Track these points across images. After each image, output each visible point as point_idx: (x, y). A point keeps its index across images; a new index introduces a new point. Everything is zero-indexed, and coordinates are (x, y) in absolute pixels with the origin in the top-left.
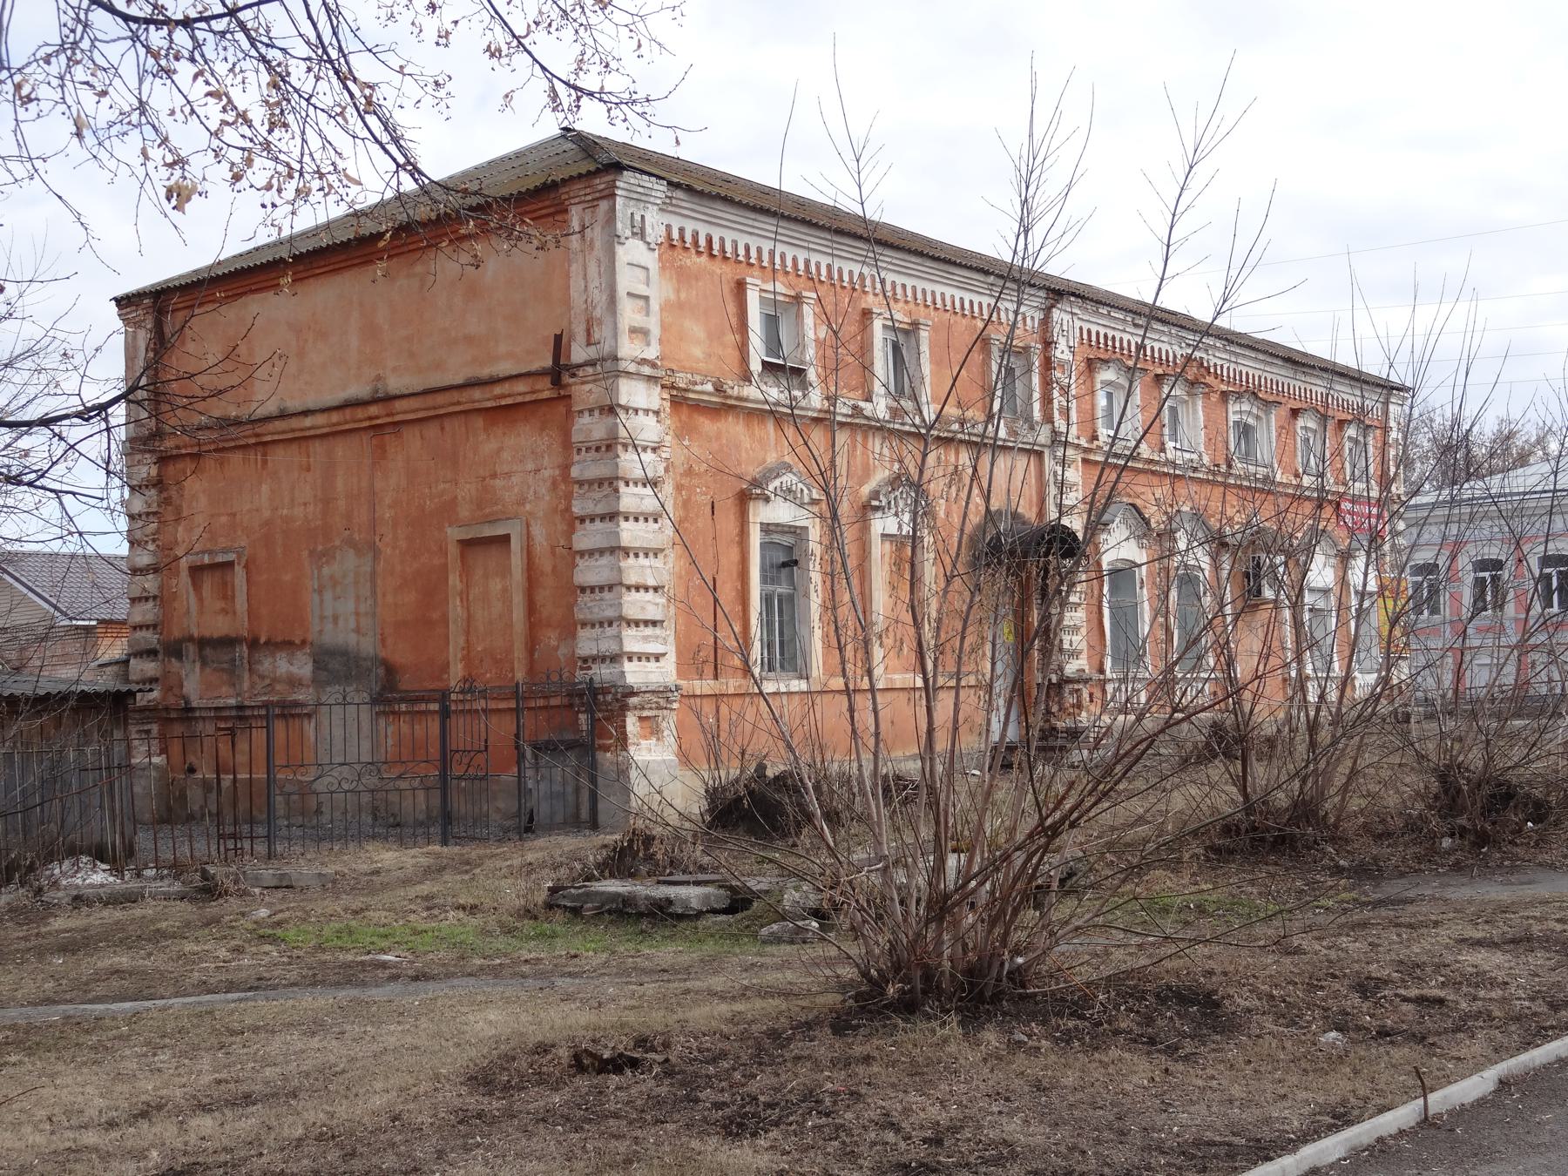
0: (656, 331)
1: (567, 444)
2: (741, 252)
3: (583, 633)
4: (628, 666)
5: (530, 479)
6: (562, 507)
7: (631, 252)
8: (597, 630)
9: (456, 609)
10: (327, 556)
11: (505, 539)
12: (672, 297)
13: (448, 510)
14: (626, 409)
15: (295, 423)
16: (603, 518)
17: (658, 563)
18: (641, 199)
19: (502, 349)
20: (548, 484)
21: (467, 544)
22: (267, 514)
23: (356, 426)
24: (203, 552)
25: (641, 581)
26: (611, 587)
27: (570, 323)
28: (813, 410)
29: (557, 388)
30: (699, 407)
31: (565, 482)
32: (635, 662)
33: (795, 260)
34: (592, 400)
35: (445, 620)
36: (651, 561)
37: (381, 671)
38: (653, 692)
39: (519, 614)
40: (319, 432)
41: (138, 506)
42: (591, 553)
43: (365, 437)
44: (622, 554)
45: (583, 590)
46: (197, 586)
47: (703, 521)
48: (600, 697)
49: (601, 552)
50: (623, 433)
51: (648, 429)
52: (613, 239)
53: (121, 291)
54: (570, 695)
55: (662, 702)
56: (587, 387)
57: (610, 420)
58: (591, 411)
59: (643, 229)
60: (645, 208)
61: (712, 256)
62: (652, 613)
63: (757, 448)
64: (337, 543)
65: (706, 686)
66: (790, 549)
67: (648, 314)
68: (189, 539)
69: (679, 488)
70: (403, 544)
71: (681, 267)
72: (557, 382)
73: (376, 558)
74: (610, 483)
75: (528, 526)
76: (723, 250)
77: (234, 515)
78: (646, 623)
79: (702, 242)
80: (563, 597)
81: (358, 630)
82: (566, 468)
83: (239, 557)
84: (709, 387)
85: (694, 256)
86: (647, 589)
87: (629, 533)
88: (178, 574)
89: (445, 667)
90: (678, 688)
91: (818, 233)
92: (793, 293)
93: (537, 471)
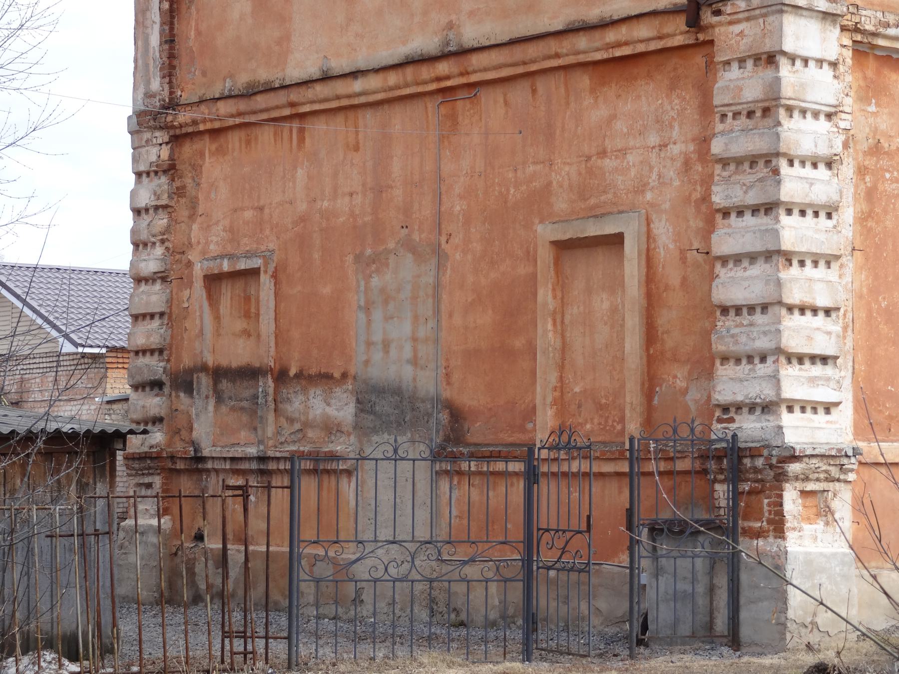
1: (706, 108)
3: (724, 372)
4: (787, 419)
5: (653, 157)
6: (696, 195)
8: (745, 367)
9: (546, 335)
10: (372, 263)
11: (617, 240)
13: (538, 201)
14: (793, 58)
16: (755, 210)
17: (832, 275)
20: (678, 164)
25: (808, 300)
26: (765, 308)
34: (743, 46)
36: (821, 272)
37: (444, 417)
38: (822, 456)
39: (633, 343)
42: (737, 259)
44: (782, 261)
45: (725, 310)
48: (747, 462)
49: (753, 257)
50: (787, 91)
55: (835, 472)
56: (737, 29)
69: (861, 171)
74: (768, 161)
75: (648, 222)
81: (414, 361)
82: (704, 142)
86: (815, 311)
89: (530, 413)
93: (663, 146)
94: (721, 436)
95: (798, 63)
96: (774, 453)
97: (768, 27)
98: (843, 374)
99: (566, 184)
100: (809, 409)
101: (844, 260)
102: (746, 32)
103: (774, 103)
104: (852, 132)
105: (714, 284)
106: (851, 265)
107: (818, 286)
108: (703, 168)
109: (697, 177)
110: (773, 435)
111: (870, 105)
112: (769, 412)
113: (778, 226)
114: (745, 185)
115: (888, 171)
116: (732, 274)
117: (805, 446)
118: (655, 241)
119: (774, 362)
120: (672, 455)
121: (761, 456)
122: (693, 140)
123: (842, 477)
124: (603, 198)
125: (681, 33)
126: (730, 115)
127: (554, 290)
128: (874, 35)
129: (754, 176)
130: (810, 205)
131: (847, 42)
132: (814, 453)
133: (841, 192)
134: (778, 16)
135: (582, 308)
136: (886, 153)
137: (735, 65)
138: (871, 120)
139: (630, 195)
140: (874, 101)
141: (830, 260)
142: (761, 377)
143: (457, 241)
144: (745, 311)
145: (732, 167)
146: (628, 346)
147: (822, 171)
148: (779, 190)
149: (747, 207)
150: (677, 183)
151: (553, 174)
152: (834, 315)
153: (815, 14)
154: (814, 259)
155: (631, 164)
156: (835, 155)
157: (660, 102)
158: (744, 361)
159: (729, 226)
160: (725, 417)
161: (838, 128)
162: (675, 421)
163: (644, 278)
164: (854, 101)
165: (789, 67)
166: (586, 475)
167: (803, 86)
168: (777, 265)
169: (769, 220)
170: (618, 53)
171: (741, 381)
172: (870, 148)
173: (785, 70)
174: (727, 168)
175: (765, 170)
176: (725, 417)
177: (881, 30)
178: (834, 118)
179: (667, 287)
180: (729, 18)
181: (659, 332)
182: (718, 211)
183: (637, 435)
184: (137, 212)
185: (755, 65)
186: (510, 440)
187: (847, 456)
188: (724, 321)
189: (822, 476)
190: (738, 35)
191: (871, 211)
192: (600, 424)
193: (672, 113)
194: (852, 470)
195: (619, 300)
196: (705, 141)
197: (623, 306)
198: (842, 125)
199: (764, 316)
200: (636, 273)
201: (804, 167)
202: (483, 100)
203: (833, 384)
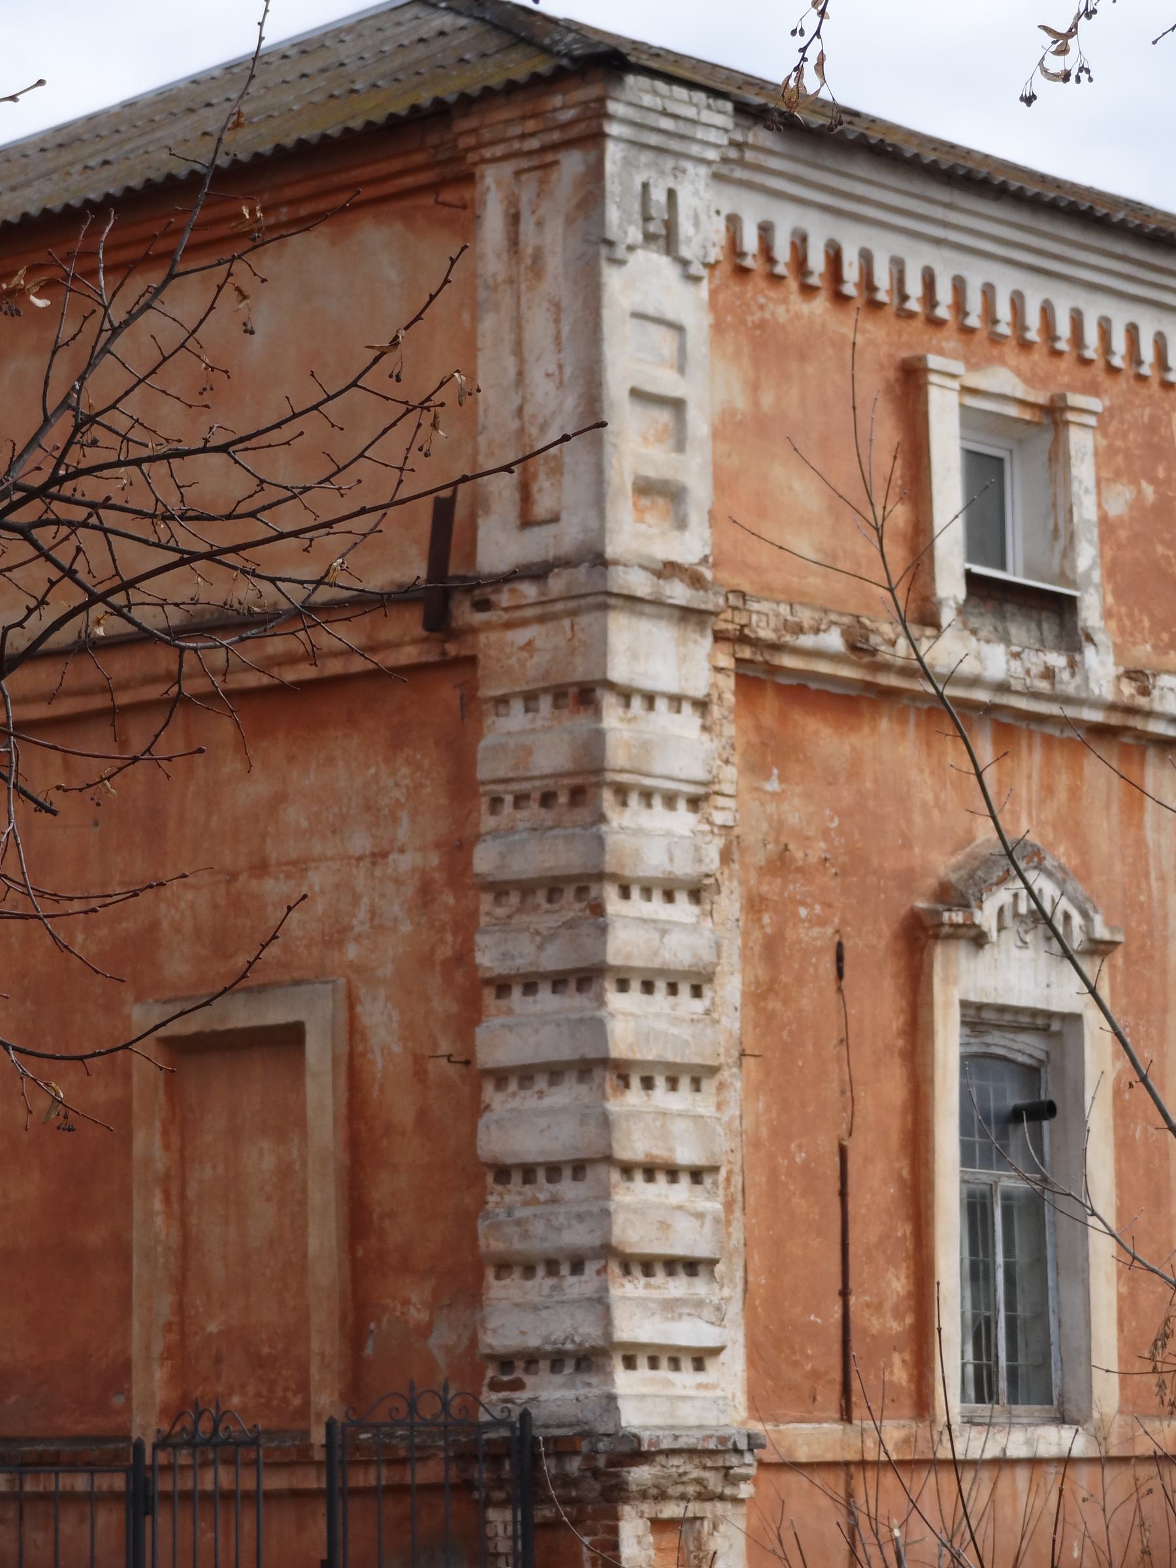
0: (700, 492)
1: (462, 784)
2: (914, 288)
3: (503, 1292)
5: (360, 879)
6: (445, 951)
7: (641, 283)
8: (541, 1283)
9: (151, 1222)
11: (291, 1037)
12: (741, 403)
14: (626, 694)
16: (558, 982)
17: (703, 1104)
18: (668, 148)
20: (409, 891)
21: (185, 1051)
25: (659, 1152)
26: (579, 1168)
28: (1095, 704)
29: (444, 635)
30: (806, 693)
31: (455, 887)
32: (643, 1370)
33: (1047, 311)
34: (534, 669)
35: (121, 1253)
36: (680, 1101)
38: (691, 1452)
39: (323, 1237)
42: (526, 1075)
44: (610, 1079)
45: (502, 1173)
47: (814, 990)
48: (549, 1466)
49: (555, 1072)
50: (617, 755)
51: (679, 747)
52: (595, 250)
54: (466, 1457)
55: (714, 1481)
56: (521, 636)
57: (581, 723)
59: (671, 226)
60: (678, 171)
61: (840, 298)
62: (688, 1239)
63: (922, 799)
65: (815, 1437)
66: (1031, 1073)
67: (680, 445)
69: (754, 905)
71: (762, 325)
72: (439, 622)
74: (582, 890)
75: (352, 1001)
76: (868, 283)
78: (672, 1265)
79: (817, 261)
80: (452, 1193)
82: (458, 849)
84: (834, 640)
85: (795, 297)
86: (673, 1173)
89: (120, 1375)
90: (754, 1442)
91: (1120, 247)
92: (1041, 398)
93: (379, 856)
94: (497, 1414)
95: (637, 703)
96: (601, 1446)
97: (580, 635)
98: (726, 1292)
100: (664, 1363)
101: (725, 1075)
102: (538, 643)
103: (593, 779)
104: (737, 831)
105: (482, 1123)
106: (738, 1085)
107: (679, 1127)
108: (457, 898)
109: (445, 917)
110: (598, 1411)
111: (768, 778)
112: (589, 1369)
113: (602, 1013)
114: (538, 933)
115: (803, 903)
116: (514, 1103)
117: (660, 1433)
119: (598, 1273)
120: (402, 1453)
121: (577, 1453)
122: (438, 845)
123: (728, 1491)
125: (414, 642)
126: (509, 799)
127: (165, 1133)
128: (776, 647)
129: (556, 916)
130: (662, 972)
131: (726, 661)
132: (676, 1446)
133: (718, 946)
134: (598, 614)
135: (220, 1169)
136: (799, 870)
137: (517, 706)
138: (771, 808)
139: (314, 950)
140: (775, 771)
141: (699, 1075)
142: (574, 1302)
144: (541, 1175)
145: (514, 899)
146: (313, 1244)
147: (683, 910)
148: (604, 944)
149: (544, 976)
150: (406, 927)
151: (163, 906)
152: (708, 1180)
153: (666, 611)
154: (670, 1074)
155: (317, 889)
156: (708, 876)
157: (373, 770)
158: (541, 1271)
159: (510, 1012)
160: (506, 1378)
161: (711, 823)
162: (412, 1388)
163: (343, 1110)
164: (740, 772)
165: (620, 711)
166: (228, 1496)
167: (646, 747)
168: (601, 1087)
169: (586, 1003)
171: (536, 1308)
172: (770, 862)
173: (612, 717)
174: (504, 900)
175: (577, 906)
176: (506, 1378)
177: (788, 638)
178: (703, 805)
180: (506, 616)
181: (375, 1217)
182: (488, 982)
183: (339, 1415)
185: (556, 706)
186: (80, 1429)
187: (736, 1450)
188: (501, 1195)
189: (691, 1490)
190: (522, 648)
191: (773, 980)
192: (258, 1395)
193: (398, 794)
194: (745, 1478)
195: (295, 1153)
196: (460, 847)
197: (304, 1163)
198: (719, 818)
199: (579, 1185)
200: (328, 1101)
201: (649, 899)
203: (707, 1313)
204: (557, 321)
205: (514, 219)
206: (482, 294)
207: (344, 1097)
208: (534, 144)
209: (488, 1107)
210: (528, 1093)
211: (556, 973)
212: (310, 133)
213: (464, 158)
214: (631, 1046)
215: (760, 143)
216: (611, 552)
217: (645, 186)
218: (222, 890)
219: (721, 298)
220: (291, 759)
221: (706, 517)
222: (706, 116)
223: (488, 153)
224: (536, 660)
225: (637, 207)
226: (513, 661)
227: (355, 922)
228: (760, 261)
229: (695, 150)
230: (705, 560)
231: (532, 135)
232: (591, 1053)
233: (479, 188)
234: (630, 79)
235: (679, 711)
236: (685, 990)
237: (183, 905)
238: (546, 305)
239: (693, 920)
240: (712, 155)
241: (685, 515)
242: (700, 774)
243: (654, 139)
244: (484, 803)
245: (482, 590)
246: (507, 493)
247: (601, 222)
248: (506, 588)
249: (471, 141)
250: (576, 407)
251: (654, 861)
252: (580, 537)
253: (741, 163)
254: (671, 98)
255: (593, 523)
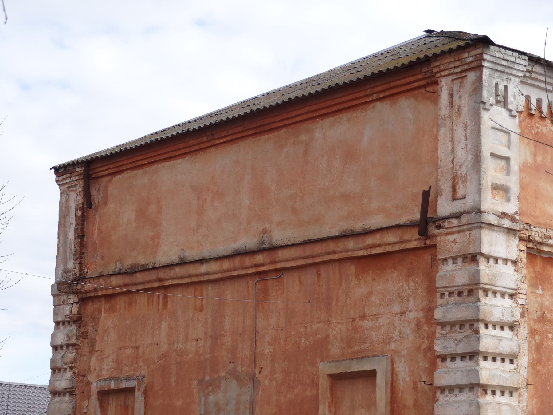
0: (515, 189)
1: (431, 289)
6: (424, 346)
7: (495, 117)
11: (372, 374)
12: (530, 160)
13: (320, 348)
15: (192, 270)
16: (463, 357)
17: (514, 401)
18: (504, 71)
19: (375, 204)
20: (413, 325)
21: (336, 378)
22: (164, 347)
23: (244, 272)
24: (110, 379)
27: (437, 180)
29: (425, 239)
34: (456, 249)
36: (505, 399)
40: (212, 277)
41: (61, 339)
42: (451, 389)
43: (251, 282)
44: (480, 390)
46: (103, 406)
49: (461, 388)
50: (484, 279)
51: (507, 277)
52: (479, 105)
53: (59, 162)
56: (451, 238)
57: (472, 267)
58: (455, 259)
59: (505, 98)
60: (508, 79)
64: (223, 374)
67: (508, 173)
68: (102, 371)
69: (533, 332)
70: (279, 376)
72: (424, 233)
73: (255, 389)
74: (472, 325)
77: (137, 348)
82: (429, 311)
83: (139, 385)
87: (488, 371)
88: (88, 397)
93: (403, 313)
95: (492, 261)
97: (472, 237)
99: (339, 336)
101: (521, 391)
102: (458, 240)
103: (476, 287)
104: (526, 307)
105: (436, 405)
106: (526, 394)
111: (538, 289)
113: (478, 368)
116: (447, 399)
118: (396, 375)
122: (423, 310)
124: (363, 346)
125: (416, 240)
126: (447, 293)
127: (329, 406)
128: (541, 244)
129: (463, 334)
130: (499, 354)
131: (523, 248)
133: (519, 346)
134: (478, 230)
136: (549, 321)
137: (450, 261)
138: (539, 299)
139: (380, 345)
143: (266, 372)
145: (448, 328)
147: (507, 333)
148: (479, 343)
149: (458, 355)
150: (412, 338)
151: (330, 330)
153: (502, 229)
154: (502, 390)
155: (382, 324)
156: (516, 321)
157: (401, 284)
159: (446, 367)
161: (517, 304)
163: (389, 400)
164: (528, 286)
165: (486, 263)
167: (494, 276)
168: (477, 393)
169: (472, 364)
170: (374, 251)
172: (538, 318)
173: (483, 265)
174: (444, 328)
175: (470, 331)
177: (545, 240)
178: (515, 297)
179: (404, 407)
180: (446, 231)
182: (439, 356)
184: (55, 348)
185: (463, 262)
190: (452, 242)
196: (430, 310)
198: (520, 302)
200: (384, 397)
202: (285, 280)
204: (466, 130)
205: (452, 96)
206: (440, 121)
207: (389, 395)
208: (458, 70)
209: (438, 400)
210: (452, 395)
211: (462, 353)
212: (383, 68)
213: (435, 76)
214: (488, 379)
215: (537, 71)
216: (483, 209)
217: (497, 84)
218: (350, 325)
219: (523, 124)
220: (374, 280)
221: (517, 198)
222: (518, 61)
223: (443, 74)
224: (457, 246)
225: (494, 91)
226: (449, 246)
227: (394, 336)
228: (537, 112)
229: (514, 72)
230: (516, 212)
231: (458, 67)
232: (473, 382)
233: (440, 85)
234: (492, 47)
235: (506, 264)
236: (507, 360)
237: (337, 329)
238: (462, 124)
239: (511, 337)
240: (520, 74)
241: (509, 197)
242: (514, 287)
243: (500, 68)
244: (439, 294)
245: (439, 222)
246: (447, 189)
247: (481, 96)
248: (447, 221)
249: (437, 70)
250: (471, 159)
251: (497, 315)
252: (472, 203)
253: (531, 78)
254: (506, 54)
255: (477, 199)
